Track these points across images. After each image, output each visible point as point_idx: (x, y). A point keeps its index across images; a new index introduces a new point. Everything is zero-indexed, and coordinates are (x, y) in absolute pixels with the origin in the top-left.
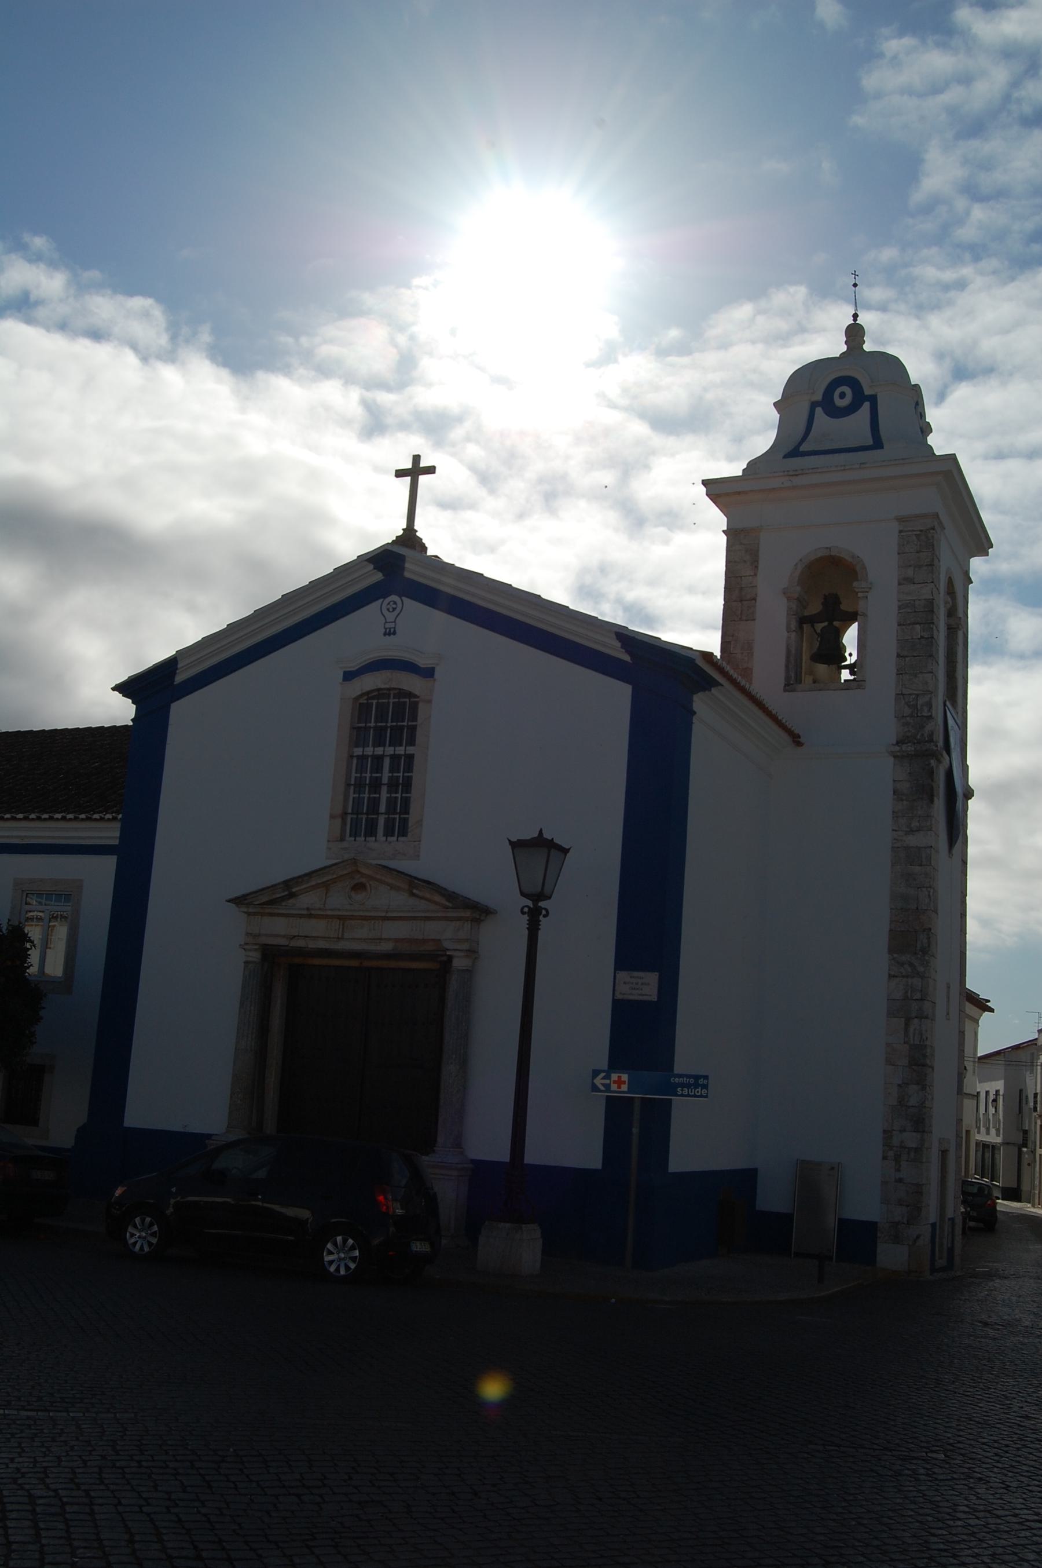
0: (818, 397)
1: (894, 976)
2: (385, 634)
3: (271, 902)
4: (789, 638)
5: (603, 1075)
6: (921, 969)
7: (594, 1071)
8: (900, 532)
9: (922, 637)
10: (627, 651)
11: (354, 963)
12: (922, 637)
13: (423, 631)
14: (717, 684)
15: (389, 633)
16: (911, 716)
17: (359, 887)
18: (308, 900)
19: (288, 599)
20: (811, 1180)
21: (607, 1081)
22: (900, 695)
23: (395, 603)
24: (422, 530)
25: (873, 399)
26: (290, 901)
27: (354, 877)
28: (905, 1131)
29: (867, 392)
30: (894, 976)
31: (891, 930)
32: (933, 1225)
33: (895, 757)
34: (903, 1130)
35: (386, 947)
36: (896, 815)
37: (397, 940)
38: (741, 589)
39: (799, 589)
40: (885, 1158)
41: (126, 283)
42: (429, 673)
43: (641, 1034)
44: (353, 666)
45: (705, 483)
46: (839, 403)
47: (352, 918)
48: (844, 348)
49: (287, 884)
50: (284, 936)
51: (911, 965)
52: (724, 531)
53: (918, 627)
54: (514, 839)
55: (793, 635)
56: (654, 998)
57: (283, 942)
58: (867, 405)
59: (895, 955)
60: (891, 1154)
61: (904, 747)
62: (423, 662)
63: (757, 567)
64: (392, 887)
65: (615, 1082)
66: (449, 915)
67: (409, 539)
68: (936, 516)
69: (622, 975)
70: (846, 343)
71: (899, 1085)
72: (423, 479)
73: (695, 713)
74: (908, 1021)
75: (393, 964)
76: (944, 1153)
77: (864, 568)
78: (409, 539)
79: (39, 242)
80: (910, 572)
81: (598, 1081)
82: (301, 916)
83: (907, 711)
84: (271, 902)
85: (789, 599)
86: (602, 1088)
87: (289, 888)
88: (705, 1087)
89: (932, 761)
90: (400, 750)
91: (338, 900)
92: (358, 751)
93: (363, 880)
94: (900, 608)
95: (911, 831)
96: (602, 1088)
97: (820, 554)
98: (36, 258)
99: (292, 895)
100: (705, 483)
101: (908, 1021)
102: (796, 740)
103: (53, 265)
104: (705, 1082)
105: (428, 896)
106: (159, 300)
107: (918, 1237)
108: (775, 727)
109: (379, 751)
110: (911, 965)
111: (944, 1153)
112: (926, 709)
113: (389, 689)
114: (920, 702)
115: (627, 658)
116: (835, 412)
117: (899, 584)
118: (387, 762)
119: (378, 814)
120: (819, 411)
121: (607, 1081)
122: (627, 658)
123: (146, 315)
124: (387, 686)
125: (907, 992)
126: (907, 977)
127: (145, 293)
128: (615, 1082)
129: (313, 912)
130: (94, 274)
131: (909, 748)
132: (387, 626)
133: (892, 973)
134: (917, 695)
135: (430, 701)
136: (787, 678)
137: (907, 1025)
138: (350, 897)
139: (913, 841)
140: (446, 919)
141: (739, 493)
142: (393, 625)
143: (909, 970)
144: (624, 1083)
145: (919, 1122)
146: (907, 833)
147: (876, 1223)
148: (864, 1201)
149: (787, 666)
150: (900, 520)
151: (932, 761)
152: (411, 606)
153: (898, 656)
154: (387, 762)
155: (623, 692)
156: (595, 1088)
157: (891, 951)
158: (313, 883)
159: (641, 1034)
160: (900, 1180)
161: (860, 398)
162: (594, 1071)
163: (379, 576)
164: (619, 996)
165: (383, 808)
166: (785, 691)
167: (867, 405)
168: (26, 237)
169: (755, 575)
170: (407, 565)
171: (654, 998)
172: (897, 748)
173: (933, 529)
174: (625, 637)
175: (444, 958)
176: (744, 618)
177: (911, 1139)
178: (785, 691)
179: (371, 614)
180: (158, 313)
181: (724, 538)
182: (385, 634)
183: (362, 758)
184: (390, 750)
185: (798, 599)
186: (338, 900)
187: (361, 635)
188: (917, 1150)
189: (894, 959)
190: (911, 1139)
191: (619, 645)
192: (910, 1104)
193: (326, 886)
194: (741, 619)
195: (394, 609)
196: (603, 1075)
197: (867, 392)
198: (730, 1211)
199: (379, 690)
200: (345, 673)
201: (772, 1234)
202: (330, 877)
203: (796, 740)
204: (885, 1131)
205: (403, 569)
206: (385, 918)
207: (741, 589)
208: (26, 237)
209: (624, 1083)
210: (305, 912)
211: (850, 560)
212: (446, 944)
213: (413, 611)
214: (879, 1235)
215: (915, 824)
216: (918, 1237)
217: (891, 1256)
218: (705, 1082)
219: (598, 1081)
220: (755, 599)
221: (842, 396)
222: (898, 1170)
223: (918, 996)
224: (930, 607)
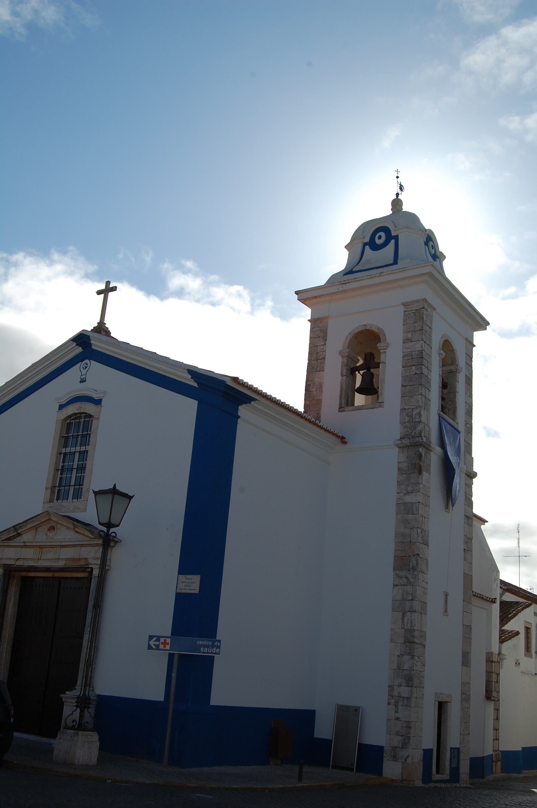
0: (367, 240)
1: (397, 585)
2: (80, 382)
3: (9, 539)
4: (342, 379)
5: (155, 638)
6: (412, 580)
7: (150, 636)
8: (405, 312)
9: (416, 374)
10: (195, 381)
11: (49, 575)
12: (416, 374)
13: (99, 377)
14: (252, 399)
15: (83, 381)
16: (409, 422)
17: (52, 528)
18: (27, 537)
19: (35, 366)
20: (348, 717)
21: (158, 643)
22: (403, 410)
23: (87, 364)
24: (109, 323)
25: (396, 238)
26: (18, 538)
27: (44, 521)
28: (401, 686)
29: (393, 234)
30: (397, 585)
31: (395, 556)
32: (427, 753)
33: (399, 447)
34: (400, 686)
35: (61, 564)
36: (399, 483)
37: (66, 559)
38: (317, 353)
39: (347, 350)
40: (389, 704)
41: (230, 280)
42: (98, 402)
43: (196, 615)
44: (63, 401)
45: (297, 293)
46: (378, 242)
47: (45, 547)
48: (391, 212)
49: (15, 528)
50: (13, 559)
51: (407, 578)
52: (308, 320)
53: (414, 367)
54: (97, 490)
55: (345, 377)
56: (197, 591)
57: (12, 562)
58: (393, 241)
59: (397, 572)
60: (393, 701)
61: (404, 441)
62: (96, 396)
63: (326, 340)
64: (68, 528)
65: (162, 643)
66: (92, 543)
67: (101, 329)
68: (425, 300)
69: (182, 577)
70: (392, 210)
71: (398, 656)
72: (110, 294)
73: (239, 417)
74: (404, 614)
75: (69, 575)
76: (442, 706)
77: (384, 335)
78: (101, 329)
79: (189, 264)
80: (410, 335)
81: (152, 643)
82: (22, 547)
83: (407, 419)
84: (9, 539)
85: (343, 357)
86: (154, 647)
87: (16, 531)
88: (219, 647)
89: (421, 449)
90: (83, 449)
91: (41, 537)
92: (63, 450)
93: (54, 524)
94: (403, 357)
95: (408, 493)
96: (154, 647)
97: (360, 329)
98: (186, 271)
99: (19, 535)
100: (297, 293)
101: (404, 614)
102: (343, 440)
103: (196, 275)
104: (219, 644)
105: (82, 532)
106: (246, 287)
107: (408, 757)
108: (322, 431)
109: (73, 449)
110: (407, 578)
111: (442, 706)
112: (417, 417)
113: (80, 413)
114: (414, 413)
115: (195, 385)
116: (375, 247)
117: (404, 343)
118: (77, 455)
119: (70, 486)
120: (367, 247)
121: (158, 643)
122: (195, 385)
123: (239, 295)
124: (78, 412)
125: (403, 595)
126: (404, 585)
127: (239, 284)
128: (162, 643)
129: (27, 544)
130: (215, 277)
131: (406, 441)
132: (82, 377)
133: (395, 583)
134: (413, 409)
135: (98, 419)
136: (341, 404)
137: (403, 616)
138: (47, 535)
139: (408, 499)
140: (91, 545)
141: (316, 297)
142: (84, 377)
143: (405, 580)
144: (168, 644)
145: (409, 681)
146: (405, 494)
147: (383, 747)
148: (375, 732)
149: (340, 397)
150: (405, 305)
151: (421, 449)
152: (95, 366)
153: (402, 386)
154: (77, 455)
155: (193, 404)
156: (150, 647)
157: (394, 569)
158: (29, 527)
159: (196, 615)
160: (397, 719)
161: (389, 237)
162: (150, 636)
163: (80, 350)
164: (179, 591)
165: (73, 483)
166: (339, 411)
167: (393, 241)
168: (183, 262)
169: (325, 344)
170: (91, 342)
171: (197, 591)
172: (400, 442)
173: (423, 308)
174: (194, 373)
175: (89, 570)
176: (318, 370)
177: (405, 691)
178: (339, 411)
179: (75, 371)
180: (245, 293)
181: (309, 324)
182: (80, 382)
183: (65, 454)
184: (78, 449)
185: (348, 356)
186: (41, 537)
187: (67, 384)
188: (408, 698)
189: (396, 574)
190: (405, 691)
191: (190, 377)
192: (404, 668)
193: (36, 528)
194: (316, 371)
195: (86, 367)
196: (155, 638)
197: (393, 234)
198: (284, 735)
199: (76, 414)
200: (60, 405)
201: (318, 753)
202: (37, 523)
203: (343, 440)
204: (389, 686)
205: (91, 344)
206: (62, 546)
207: (317, 353)
208: (183, 262)
209: (168, 644)
210: (23, 544)
211: (377, 331)
212: (91, 561)
213: (96, 368)
214: (384, 755)
215: (410, 489)
216: (408, 757)
217: (391, 770)
218: (219, 644)
219: (152, 643)
220: (324, 358)
221: (380, 237)
222: (397, 712)
223: (410, 598)
224: (421, 355)
